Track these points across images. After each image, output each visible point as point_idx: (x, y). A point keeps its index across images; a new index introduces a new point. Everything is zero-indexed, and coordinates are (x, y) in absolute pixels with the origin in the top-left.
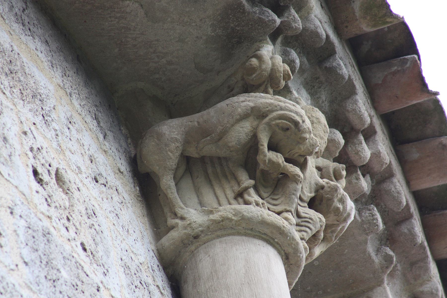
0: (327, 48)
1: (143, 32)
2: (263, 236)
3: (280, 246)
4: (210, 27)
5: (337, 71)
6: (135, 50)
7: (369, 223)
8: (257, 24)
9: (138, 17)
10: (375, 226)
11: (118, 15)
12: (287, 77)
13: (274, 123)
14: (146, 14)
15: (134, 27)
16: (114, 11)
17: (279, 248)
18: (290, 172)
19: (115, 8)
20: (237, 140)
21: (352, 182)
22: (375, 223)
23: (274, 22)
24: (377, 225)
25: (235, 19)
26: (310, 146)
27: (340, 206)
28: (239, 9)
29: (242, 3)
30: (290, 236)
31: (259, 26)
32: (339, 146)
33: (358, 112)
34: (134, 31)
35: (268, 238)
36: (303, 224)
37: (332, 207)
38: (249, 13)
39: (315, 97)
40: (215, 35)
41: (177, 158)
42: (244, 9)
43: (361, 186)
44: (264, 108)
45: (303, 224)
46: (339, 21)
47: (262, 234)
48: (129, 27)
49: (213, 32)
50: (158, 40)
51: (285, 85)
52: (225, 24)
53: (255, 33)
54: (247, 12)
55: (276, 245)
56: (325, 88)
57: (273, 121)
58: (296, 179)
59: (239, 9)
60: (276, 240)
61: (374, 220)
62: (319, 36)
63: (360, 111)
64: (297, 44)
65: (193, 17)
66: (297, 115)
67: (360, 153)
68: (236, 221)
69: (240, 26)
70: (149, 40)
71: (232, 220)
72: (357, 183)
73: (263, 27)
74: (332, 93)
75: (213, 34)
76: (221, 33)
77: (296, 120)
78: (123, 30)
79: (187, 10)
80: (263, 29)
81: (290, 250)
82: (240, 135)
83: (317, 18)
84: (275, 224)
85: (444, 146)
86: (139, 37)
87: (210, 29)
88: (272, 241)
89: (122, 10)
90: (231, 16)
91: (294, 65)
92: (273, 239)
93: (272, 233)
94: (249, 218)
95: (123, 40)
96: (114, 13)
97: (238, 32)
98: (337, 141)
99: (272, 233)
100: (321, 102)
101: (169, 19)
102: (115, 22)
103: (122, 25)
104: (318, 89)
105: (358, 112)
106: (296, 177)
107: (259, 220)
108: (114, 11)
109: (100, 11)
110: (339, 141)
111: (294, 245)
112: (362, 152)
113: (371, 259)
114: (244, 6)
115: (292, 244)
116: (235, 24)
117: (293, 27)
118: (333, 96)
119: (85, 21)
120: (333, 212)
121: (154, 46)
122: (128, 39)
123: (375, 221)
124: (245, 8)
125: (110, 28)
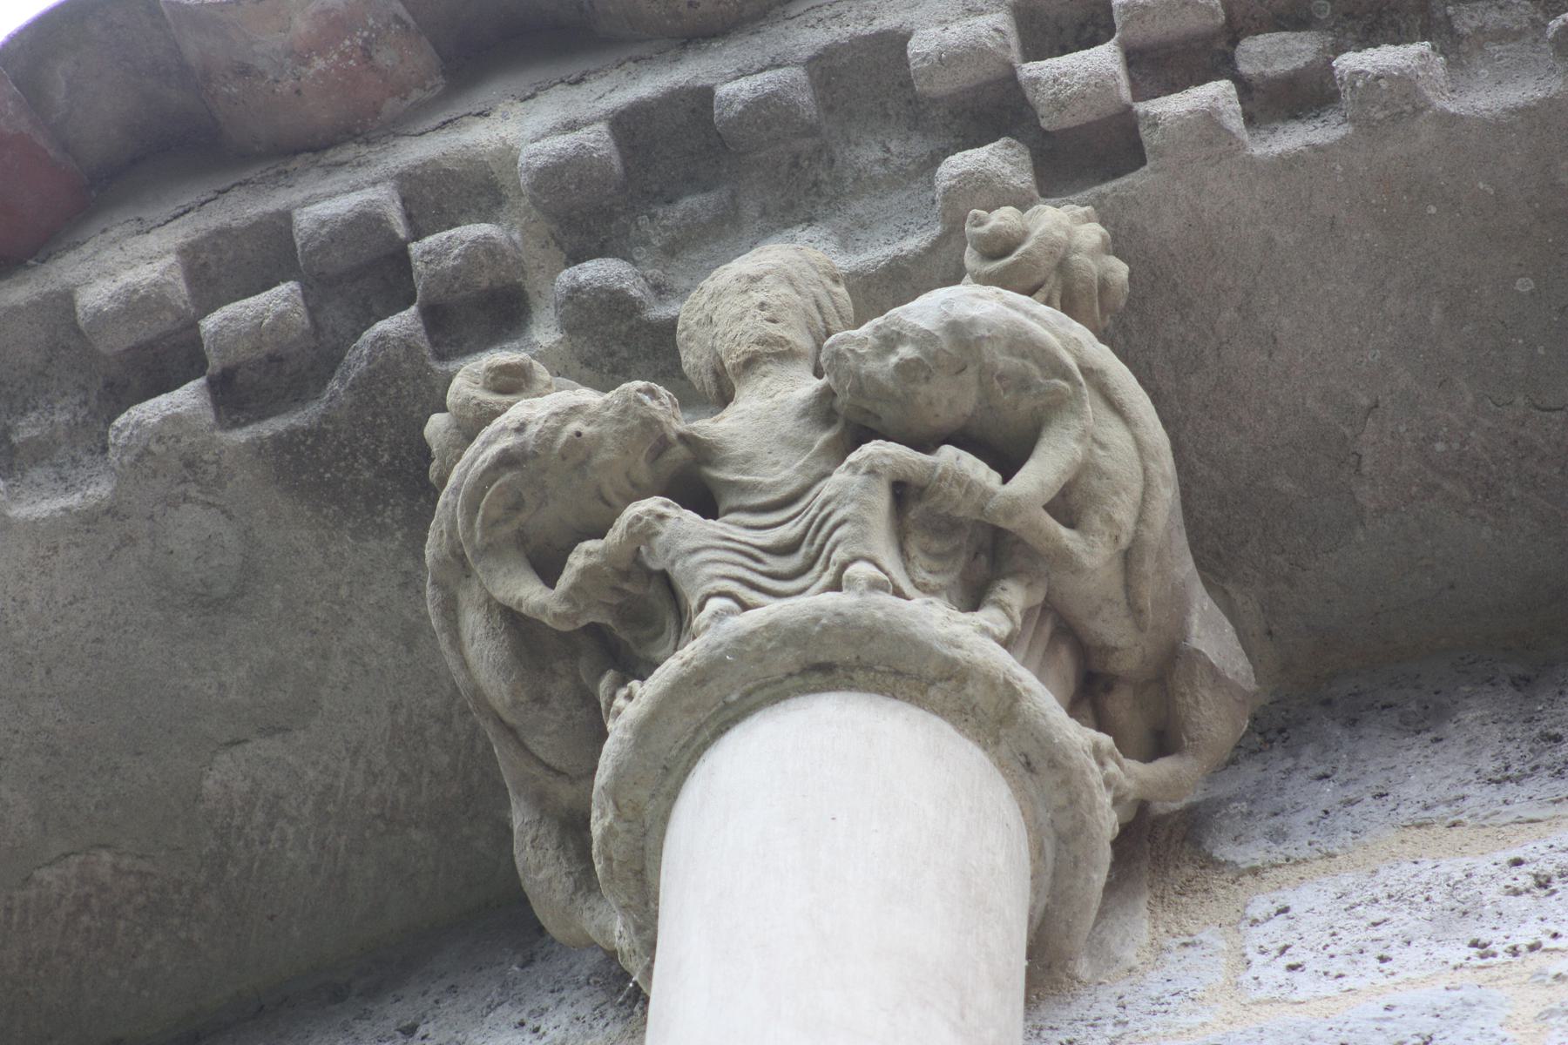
0: (694, 111)
1: (347, 749)
2: (700, 740)
3: (766, 685)
4: (367, 541)
5: (730, 120)
6: (427, 780)
7: (1361, 102)
8: (374, 397)
9: (278, 759)
10: (1379, 86)
11: (259, 817)
12: (504, 379)
13: (478, 535)
14: (270, 731)
15: (321, 772)
16: (240, 829)
17: (767, 692)
18: (620, 543)
19: (229, 825)
20: (495, 673)
21: (1157, 147)
22: (1367, 85)
23: (380, 343)
24: (1378, 78)
25: (343, 464)
26: (620, 421)
27: (906, 352)
28: (302, 448)
29: (282, 433)
30: (727, 651)
31: (383, 394)
32: (977, 180)
33: (926, 64)
34: (336, 775)
35: (713, 726)
36: (818, 541)
37: (891, 384)
38: (328, 416)
39: (847, 190)
40: (406, 530)
41: (558, 858)
42: (307, 432)
43: (1180, 118)
44: (439, 545)
45: (818, 541)
46: (668, 22)
47: (694, 739)
48: (319, 788)
49: (393, 534)
50: (394, 708)
51: (1235, 68)
52: (359, 497)
53: (416, 409)
54: (320, 423)
55: (749, 702)
56: (849, 142)
57: (473, 536)
58: (640, 532)
59: (302, 448)
60: (734, 697)
61: (1355, 83)
62: (555, 166)
63: (924, 60)
64: (622, 219)
65: (312, 589)
66: (494, 442)
67: (1062, 97)
68: (618, 817)
69: (375, 450)
70: (388, 734)
71: (611, 827)
72: (1164, 129)
73: (395, 380)
74: (886, 116)
75: (399, 535)
76: (398, 511)
77: (493, 457)
78: (330, 808)
79: (277, 604)
80: (403, 379)
81: (789, 658)
82: (485, 657)
83: (544, 136)
84: (660, 694)
85: (690, 5)
86: (369, 762)
87: (373, 544)
88: (730, 714)
89: (240, 804)
90: (328, 475)
91: (588, 293)
92: (727, 706)
93: (690, 710)
94: (615, 775)
95: (375, 811)
96: (247, 829)
97: (404, 458)
98: (953, 182)
99: (690, 710)
100: (878, 170)
101: (309, 664)
102: (291, 831)
103: (306, 810)
104: (834, 170)
105: (926, 64)
106: (635, 530)
107: (632, 742)
108: (240, 829)
109: (233, 871)
110: (959, 175)
111: (769, 640)
112: (1067, 85)
113: (1535, 109)
114: (292, 432)
115: (759, 648)
116: (362, 464)
117: (454, 267)
118: (898, 114)
119: (271, 918)
120: (912, 387)
121: (415, 719)
122: (373, 797)
123: (1359, 84)
124: (303, 427)
125: (311, 847)
